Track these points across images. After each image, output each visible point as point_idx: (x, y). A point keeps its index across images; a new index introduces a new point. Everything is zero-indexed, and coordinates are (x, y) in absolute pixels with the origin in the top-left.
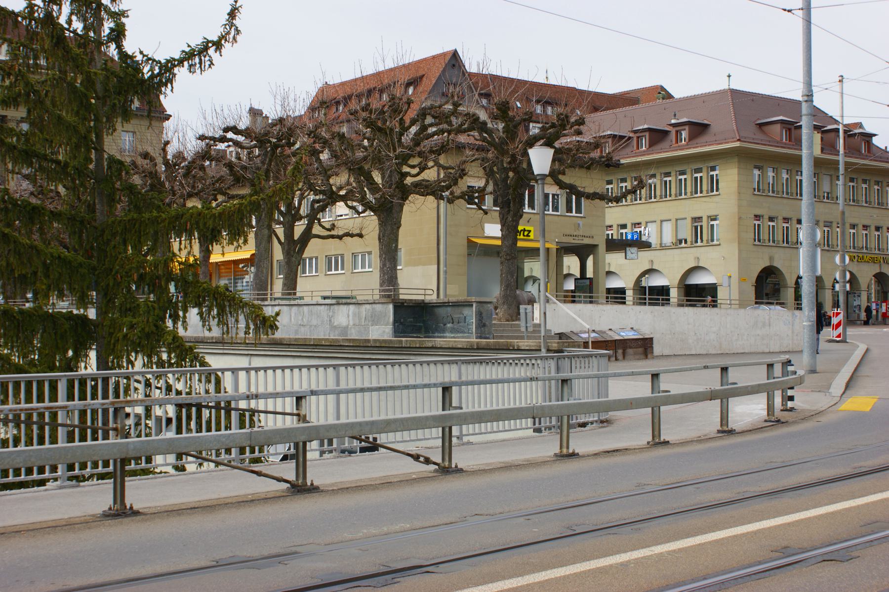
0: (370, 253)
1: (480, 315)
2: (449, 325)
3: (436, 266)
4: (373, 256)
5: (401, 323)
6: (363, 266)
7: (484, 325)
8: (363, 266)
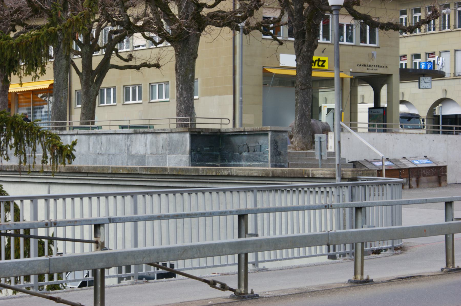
0: (167, 83)
1: (275, 143)
2: (244, 154)
3: (232, 96)
4: (170, 86)
5: (198, 152)
6: (160, 96)
7: (280, 154)
8: (160, 96)
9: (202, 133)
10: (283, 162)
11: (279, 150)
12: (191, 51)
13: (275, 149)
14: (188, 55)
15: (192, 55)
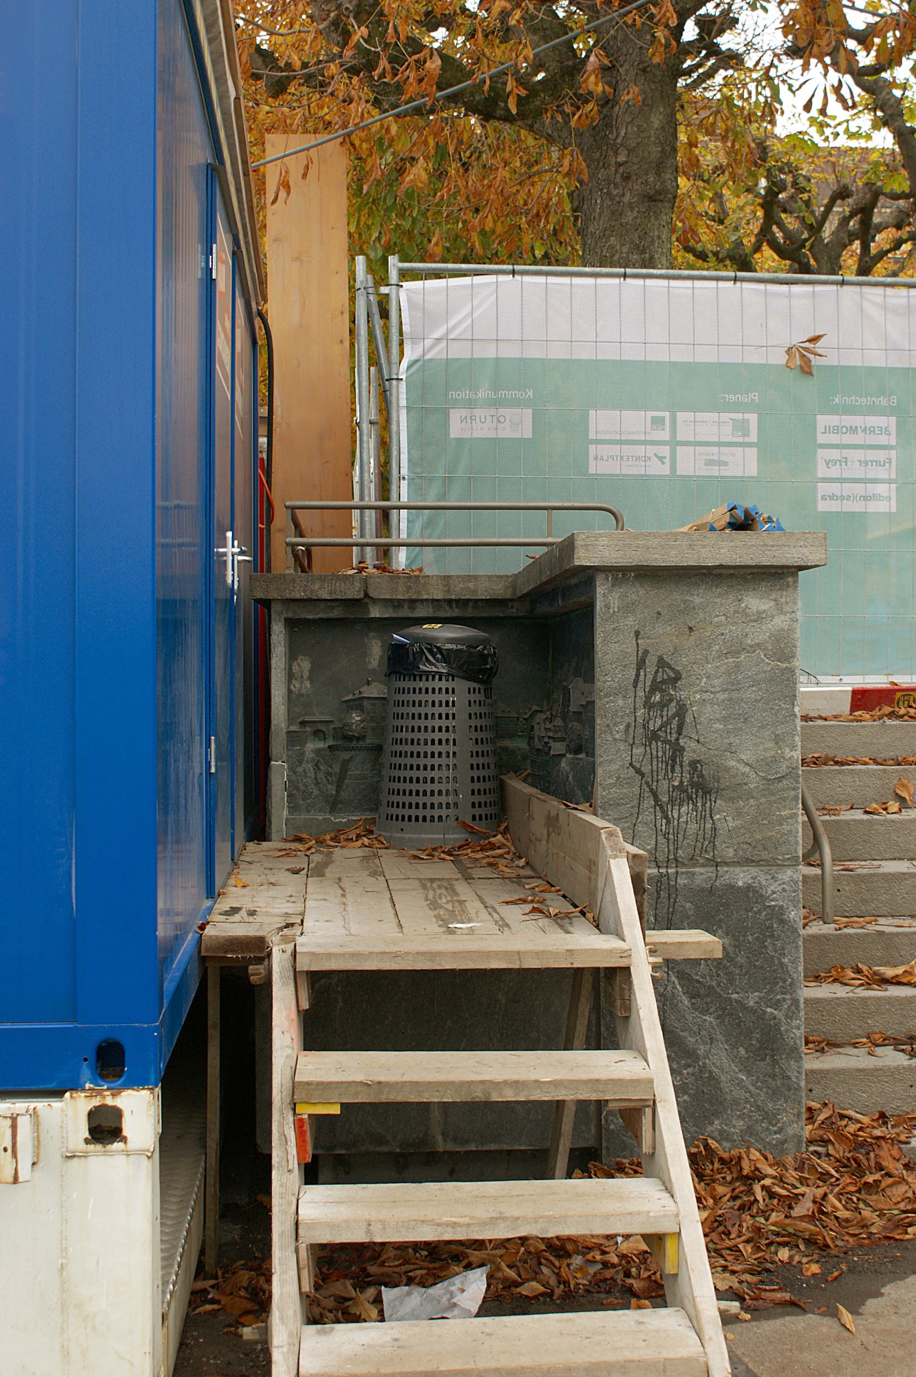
7: (701, 787)
9: (375, 612)
10: (747, 862)
11: (691, 749)
12: (622, 158)
13: (654, 736)
14: (608, 181)
15: (627, 178)
